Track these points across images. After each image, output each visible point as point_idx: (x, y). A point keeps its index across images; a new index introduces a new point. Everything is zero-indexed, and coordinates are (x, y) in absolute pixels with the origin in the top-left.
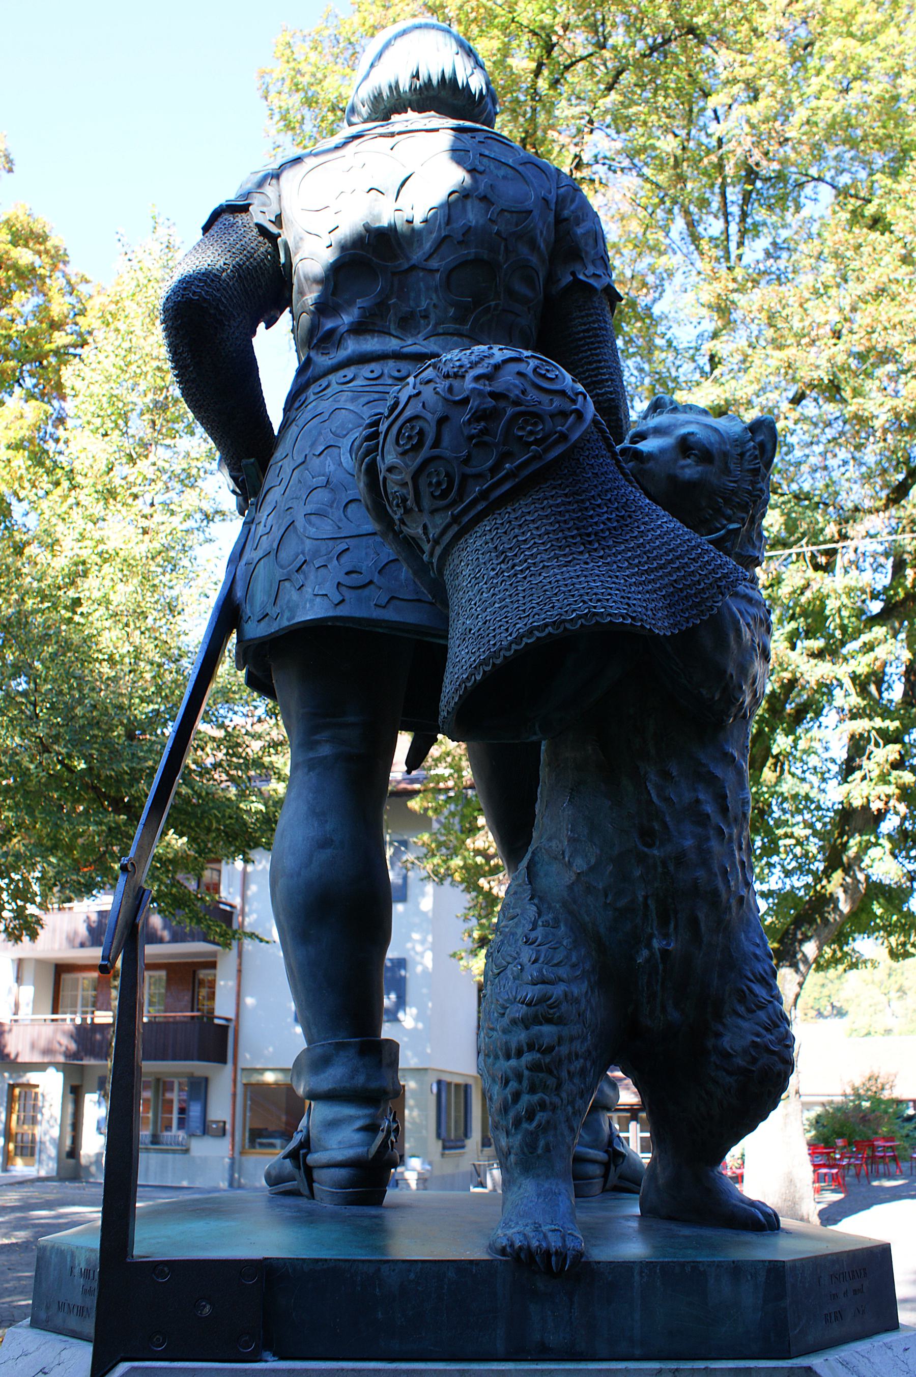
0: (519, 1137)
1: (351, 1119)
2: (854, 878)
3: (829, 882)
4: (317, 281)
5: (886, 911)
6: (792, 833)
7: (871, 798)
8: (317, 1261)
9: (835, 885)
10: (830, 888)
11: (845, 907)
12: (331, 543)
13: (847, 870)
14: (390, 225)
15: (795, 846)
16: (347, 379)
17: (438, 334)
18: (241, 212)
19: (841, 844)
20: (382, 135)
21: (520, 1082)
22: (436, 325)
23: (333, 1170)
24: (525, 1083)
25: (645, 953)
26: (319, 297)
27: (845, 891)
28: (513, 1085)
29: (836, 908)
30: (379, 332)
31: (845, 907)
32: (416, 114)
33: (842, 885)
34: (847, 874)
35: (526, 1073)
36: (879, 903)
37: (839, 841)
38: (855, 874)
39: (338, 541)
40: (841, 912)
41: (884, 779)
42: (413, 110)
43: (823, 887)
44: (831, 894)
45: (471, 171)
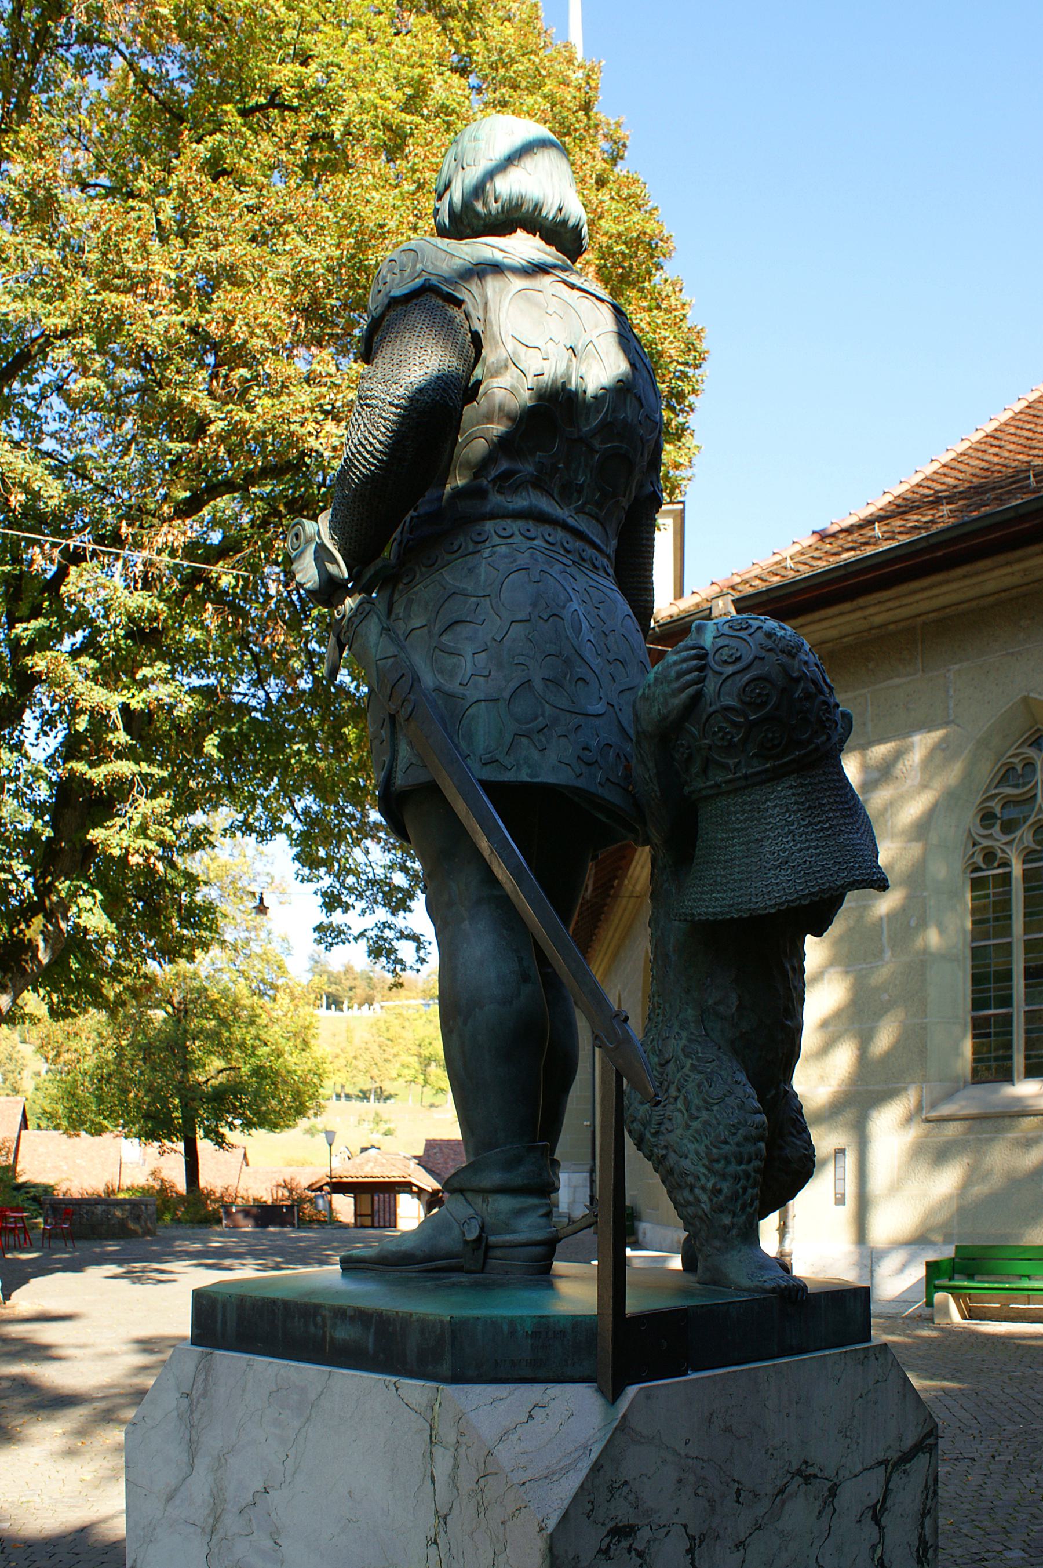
0: (744, 1217)
1: (535, 1207)
2: (57, 926)
3: (28, 927)
4: (510, 417)
5: (83, 967)
6: (10, 866)
7: (131, 850)
8: (703, 1306)
9: (35, 930)
10: (29, 934)
11: (44, 957)
12: (568, 715)
13: (49, 916)
14: (554, 381)
15: (10, 881)
16: (528, 534)
17: (584, 513)
18: (455, 305)
19: (44, 884)
20: (565, 282)
21: (748, 1180)
22: (585, 504)
23: (529, 1249)
24: (751, 1181)
25: (773, 1092)
26: (507, 432)
27: (45, 940)
28: (743, 1182)
29: (35, 957)
30: (547, 491)
31: (44, 957)
32: (543, 243)
33: (42, 932)
34: (49, 921)
35: (753, 1174)
36: (76, 957)
37: (41, 882)
38: (57, 922)
39: (574, 716)
40: (40, 962)
41: (142, 831)
42: (542, 238)
43: (21, 931)
44: (30, 940)
45: (633, 365)
